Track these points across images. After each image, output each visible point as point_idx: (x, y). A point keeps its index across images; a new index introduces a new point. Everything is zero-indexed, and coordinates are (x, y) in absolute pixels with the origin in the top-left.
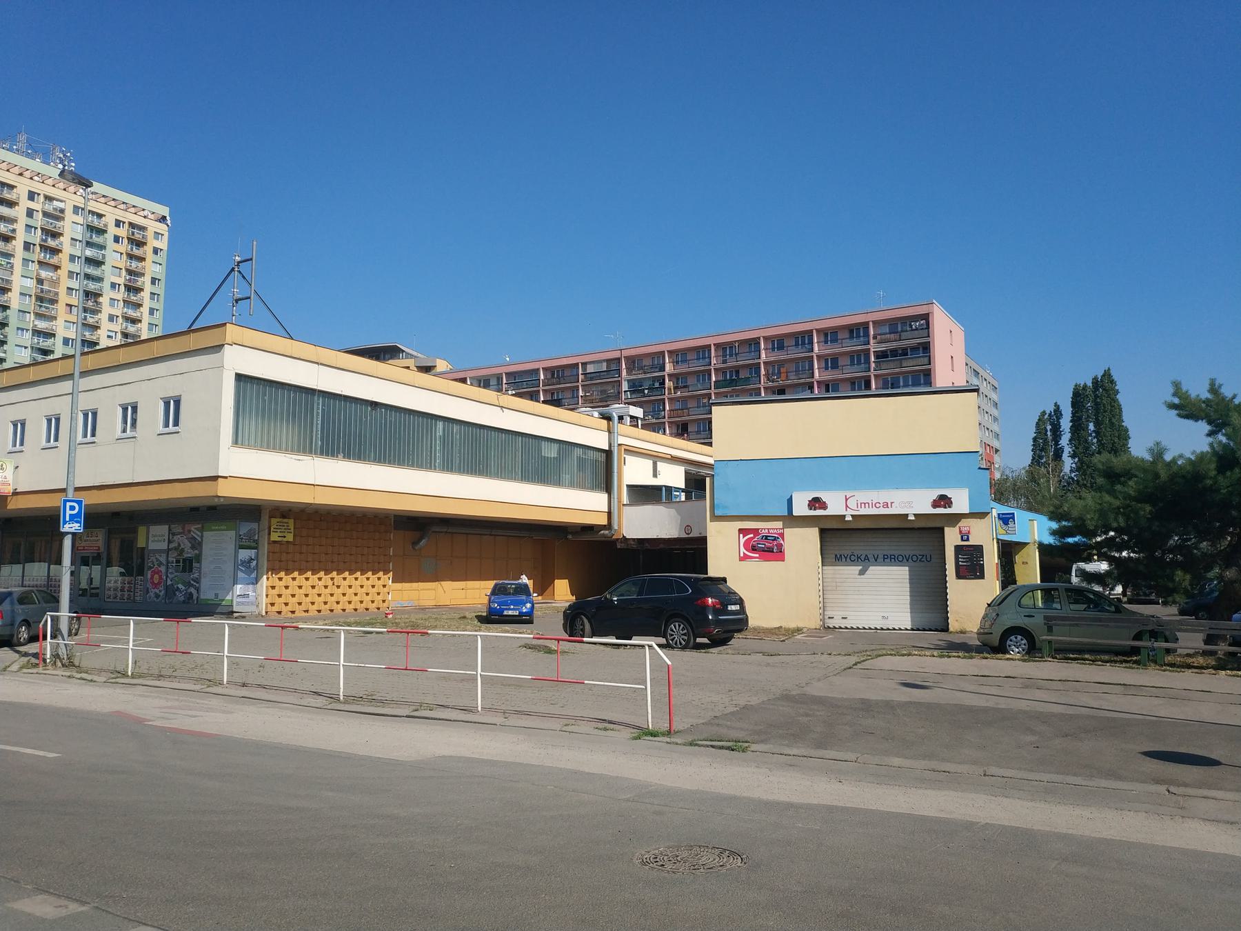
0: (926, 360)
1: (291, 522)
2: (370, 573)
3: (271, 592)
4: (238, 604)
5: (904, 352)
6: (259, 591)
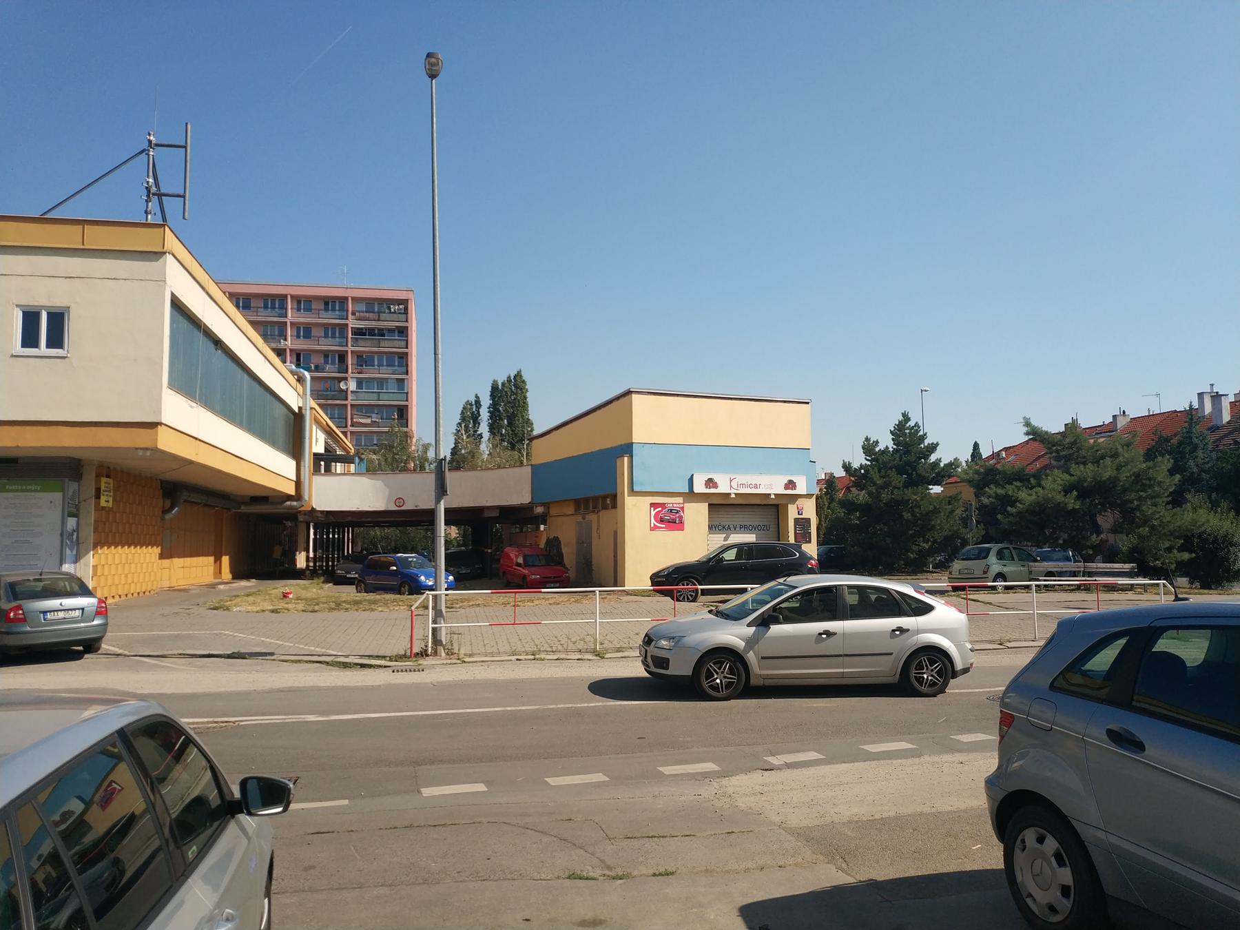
0: (403, 343)
5: (382, 332)
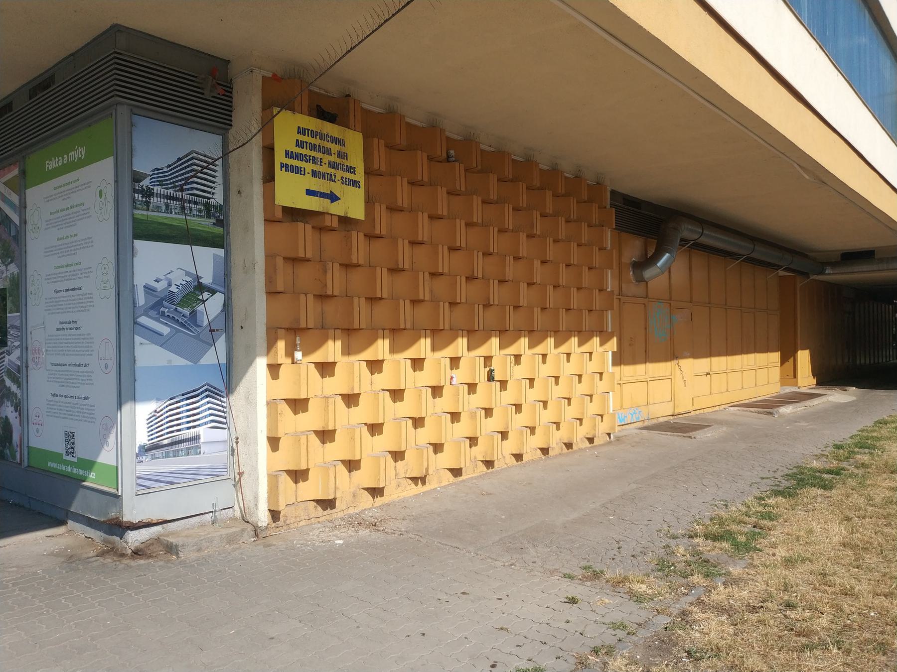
1: (354, 142)
2: (461, 343)
3: (290, 422)
4: (145, 485)
6: (239, 422)
